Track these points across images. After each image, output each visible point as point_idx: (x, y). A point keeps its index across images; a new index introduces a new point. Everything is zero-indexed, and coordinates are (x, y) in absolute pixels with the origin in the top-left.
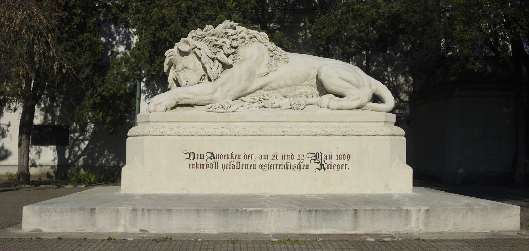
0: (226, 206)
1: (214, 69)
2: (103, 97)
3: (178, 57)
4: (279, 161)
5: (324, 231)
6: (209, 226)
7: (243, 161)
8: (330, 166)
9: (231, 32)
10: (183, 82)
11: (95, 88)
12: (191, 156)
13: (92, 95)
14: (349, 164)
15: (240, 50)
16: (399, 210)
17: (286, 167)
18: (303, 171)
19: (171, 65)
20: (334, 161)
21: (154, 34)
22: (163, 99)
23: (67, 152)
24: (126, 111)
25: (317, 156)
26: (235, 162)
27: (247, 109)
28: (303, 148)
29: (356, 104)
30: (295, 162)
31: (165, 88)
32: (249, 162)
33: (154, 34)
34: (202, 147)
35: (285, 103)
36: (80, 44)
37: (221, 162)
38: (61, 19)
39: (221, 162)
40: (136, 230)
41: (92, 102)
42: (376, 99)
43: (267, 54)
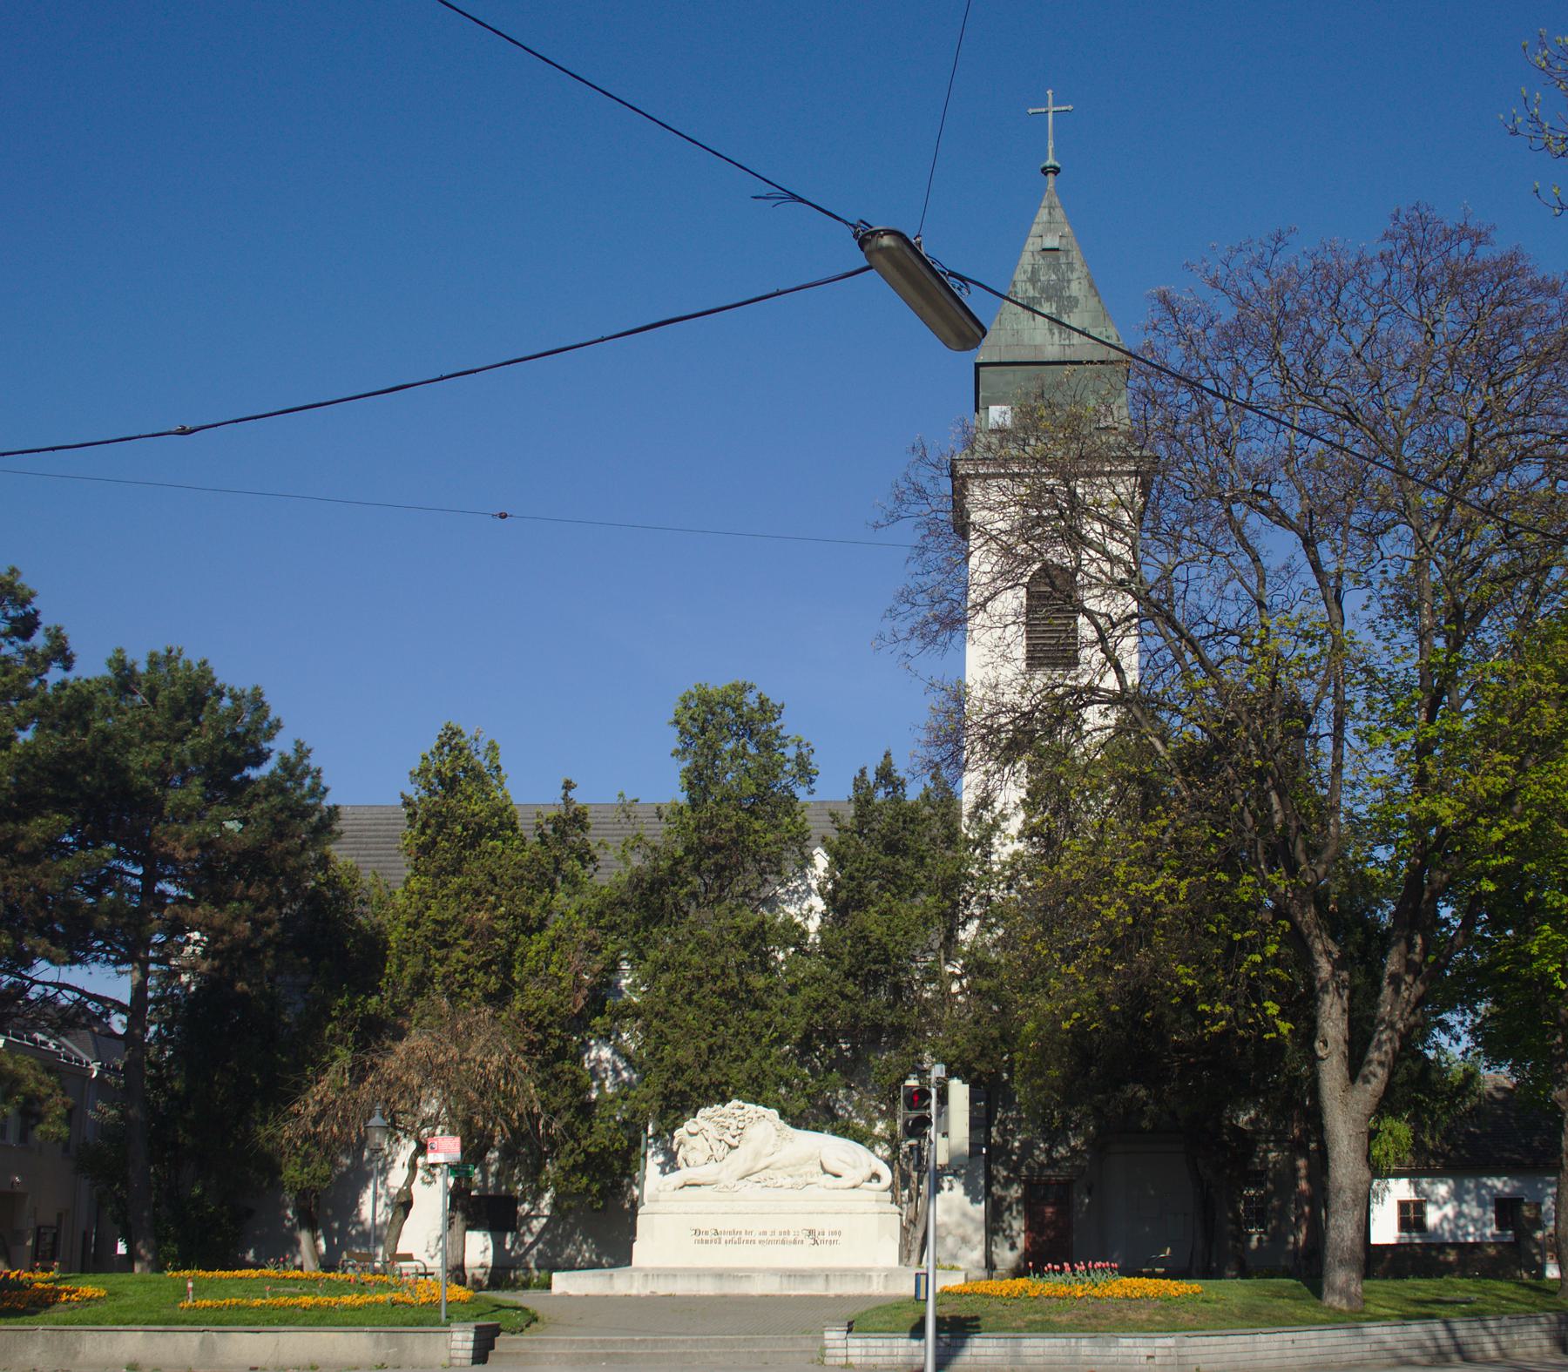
0: (719, 1275)
1: (720, 1149)
2: (588, 1154)
3: (687, 1137)
4: (777, 1237)
5: (802, 1292)
6: (707, 1288)
7: (744, 1237)
8: (823, 1242)
9: (738, 1112)
10: (691, 1163)
11: (578, 1141)
12: (697, 1232)
13: (572, 1151)
14: (840, 1240)
15: (747, 1131)
16: (863, 1276)
17: (783, 1242)
18: (799, 1246)
19: (680, 1144)
20: (827, 1237)
21: (666, 1086)
22: (675, 1178)
23: (509, 1237)
24: (624, 1175)
25: (811, 1232)
26: (736, 1238)
27: (749, 1189)
28: (799, 1224)
29: (851, 1184)
30: (791, 1238)
31: (675, 1168)
32: (749, 1238)
33: (666, 1086)
34: (707, 1224)
35: (788, 1182)
36: (556, 1077)
37: (724, 1238)
38: (531, 1043)
39: (724, 1238)
40: (647, 1292)
41: (571, 1161)
42: (876, 1176)
43: (775, 1133)
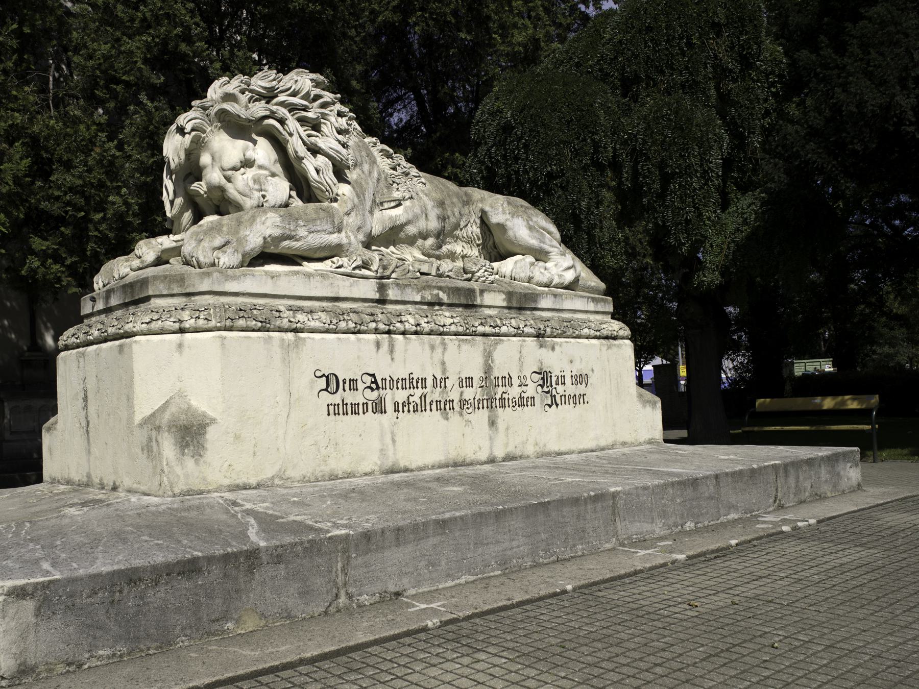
12: (331, 382)
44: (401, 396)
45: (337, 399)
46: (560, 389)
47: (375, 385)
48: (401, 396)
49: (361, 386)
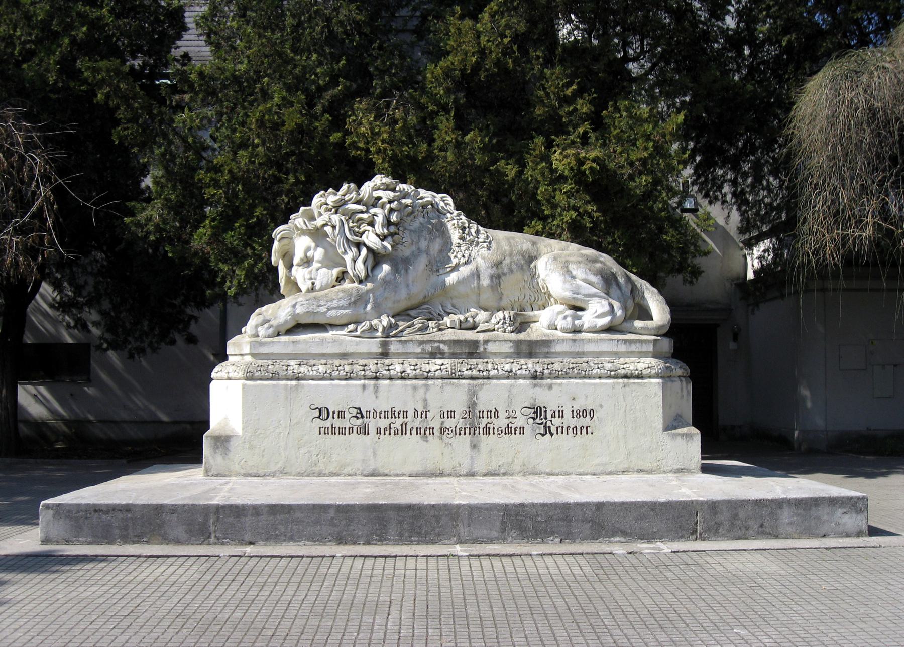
12: (322, 412)
20: (569, 420)
30: (502, 422)
44: (383, 423)
45: (328, 424)
46: (557, 421)
47: (360, 414)
48: (383, 423)
49: (347, 415)
